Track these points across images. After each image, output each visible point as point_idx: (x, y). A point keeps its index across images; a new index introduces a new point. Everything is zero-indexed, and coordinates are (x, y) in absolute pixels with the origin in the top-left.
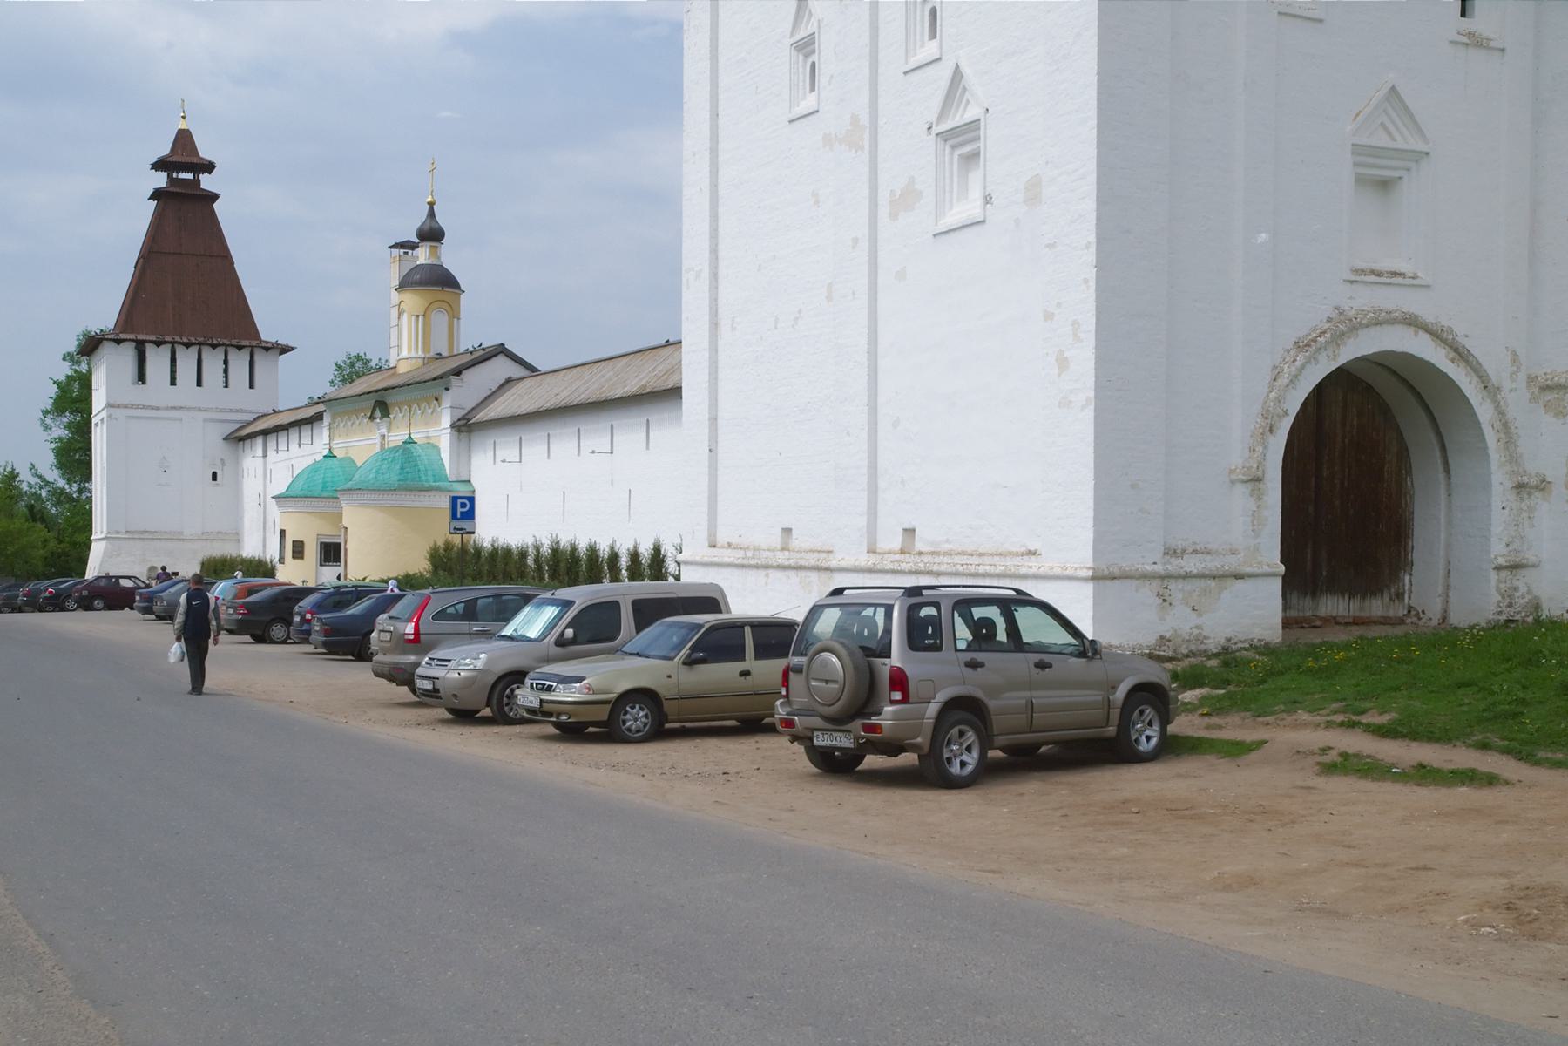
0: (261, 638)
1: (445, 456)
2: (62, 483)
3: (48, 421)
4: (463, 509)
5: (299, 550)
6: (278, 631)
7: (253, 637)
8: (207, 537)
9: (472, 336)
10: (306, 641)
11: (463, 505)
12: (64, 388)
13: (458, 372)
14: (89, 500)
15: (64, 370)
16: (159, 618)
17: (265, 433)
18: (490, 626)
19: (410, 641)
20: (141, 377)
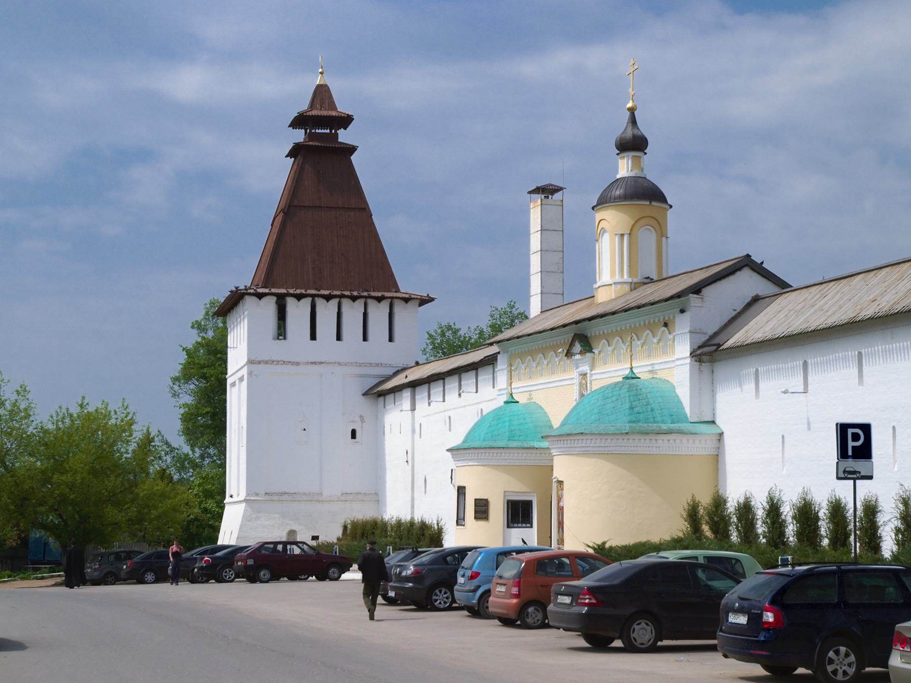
1: (684, 393)
2: (186, 449)
3: (176, 388)
8: (346, 497)
15: (192, 338)
17: (414, 385)
20: (281, 332)
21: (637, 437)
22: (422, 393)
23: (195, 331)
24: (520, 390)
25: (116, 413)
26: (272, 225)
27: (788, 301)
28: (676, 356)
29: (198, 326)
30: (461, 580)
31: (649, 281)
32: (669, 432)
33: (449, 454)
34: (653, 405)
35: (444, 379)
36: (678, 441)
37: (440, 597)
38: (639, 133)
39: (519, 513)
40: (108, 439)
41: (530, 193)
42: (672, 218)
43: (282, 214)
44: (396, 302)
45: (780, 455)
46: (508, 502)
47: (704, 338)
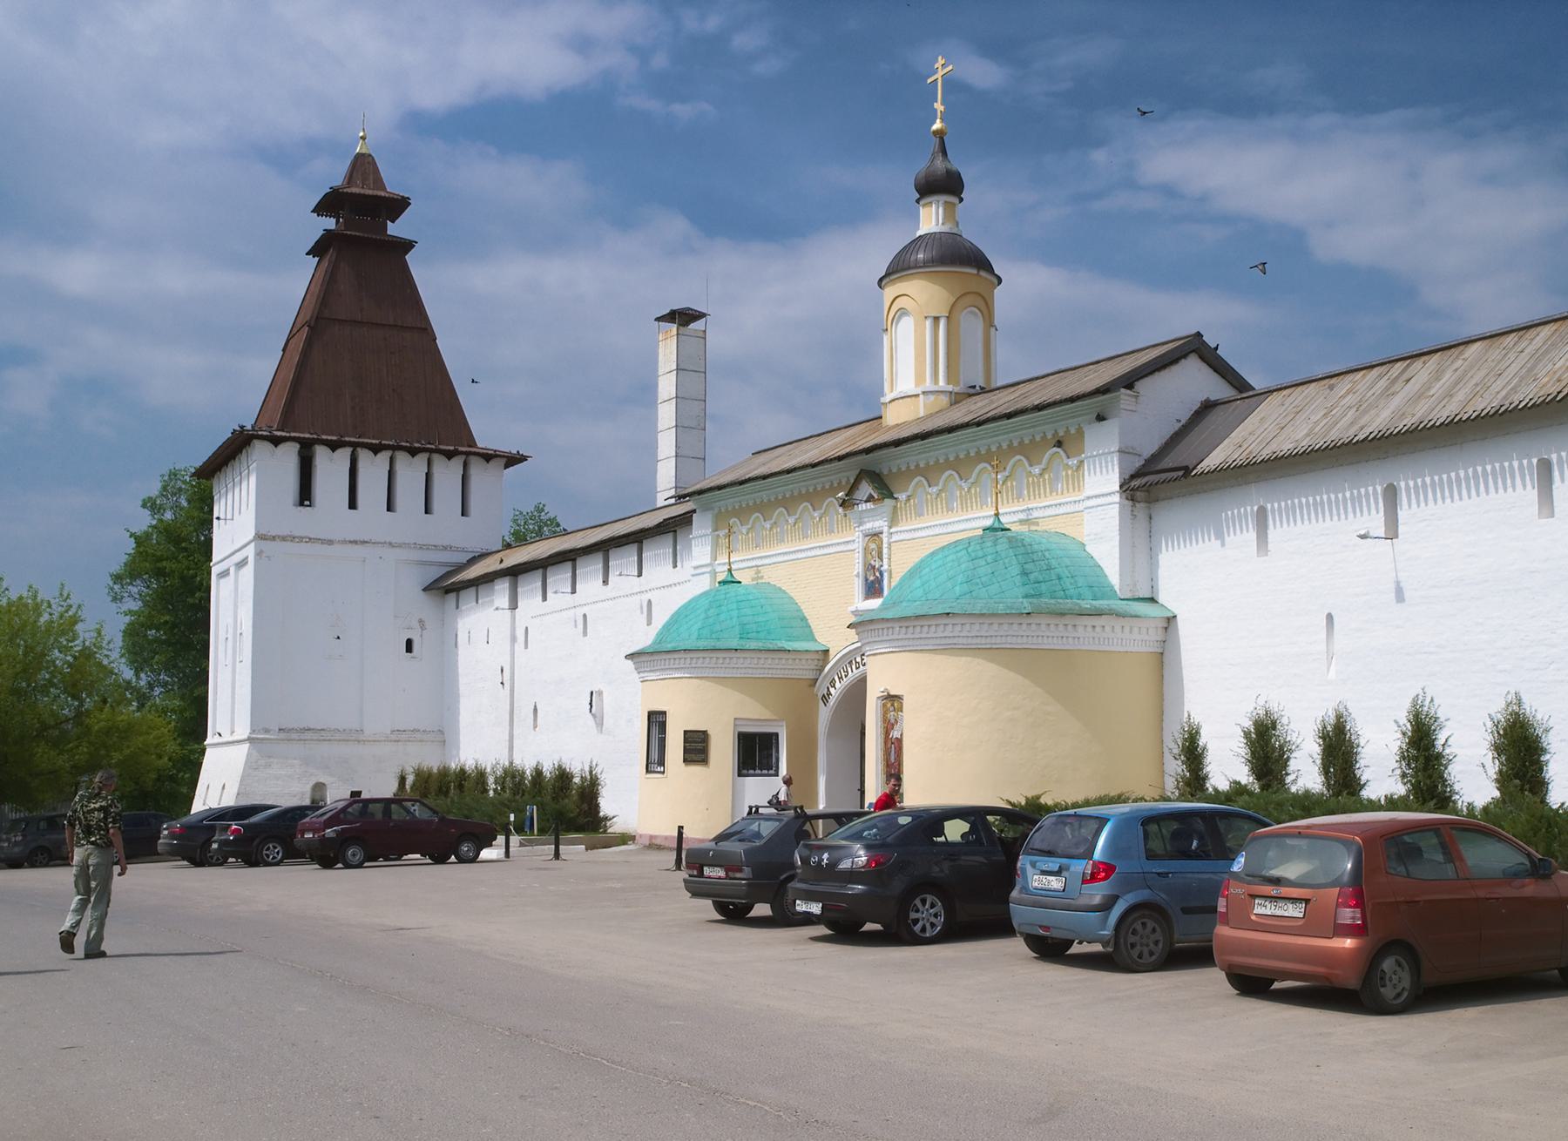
2: (128, 674)
8: (399, 736)
13: (1129, 381)
20: (305, 494)
21: (1044, 620)
27: (1269, 409)
28: (1088, 492)
29: (151, 505)
31: (973, 392)
32: (1098, 613)
33: (629, 662)
36: (1118, 629)
39: (755, 752)
41: (658, 319)
47: (1138, 463)
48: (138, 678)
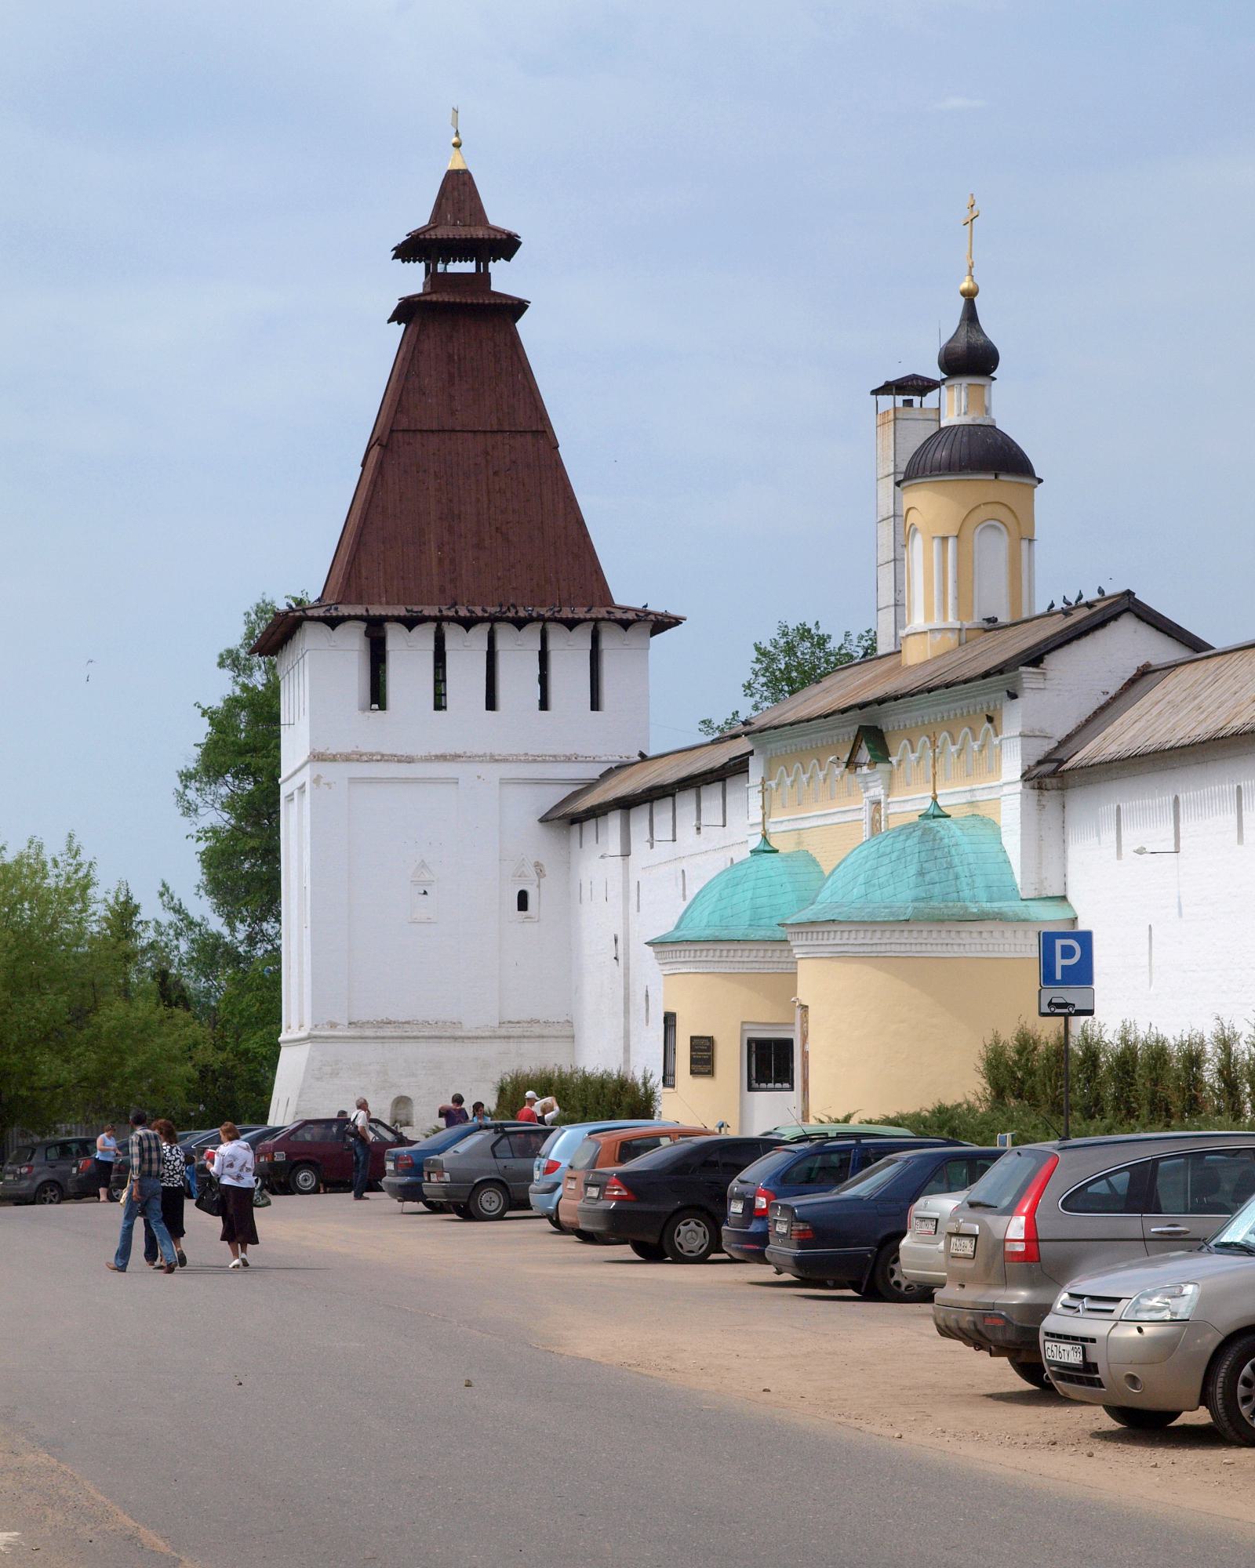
0: (653, 1252)
1: (1012, 842)
2: (216, 924)
3: (191, 794)
4: (1067, 961)
5: (703, 1057)
6: (691, 1235)
7: (638, 1247)
8: (508, 1032)
9: (1063, 575)
10: (760, 1258)
11: (1068, 952)
12: (221, 721)
13: (1035, 658)
14: (275, 956)
15: (221, 687)
16: (435, 1208)
17: (625, 804)
18: (1187, 1223)
19: (1016, 1255)
20: (377, 696)
22: (639, 819)
23: (228, 674)
24: (783, 827)
25: (56, 864)
26: (363, 465)
28: (1004, 780)
30: (537, 1175)
34: (959, 869)
35: (673, 795)
37: (691, 1235)
38: (981, 340)
40: (43, 915)
41: (875, 392)
42: (1047, 503)
43: (377, 448)
44: (602, 625)
45: (1145, 960)
46: (750, 1041)
48: (233, 930)
